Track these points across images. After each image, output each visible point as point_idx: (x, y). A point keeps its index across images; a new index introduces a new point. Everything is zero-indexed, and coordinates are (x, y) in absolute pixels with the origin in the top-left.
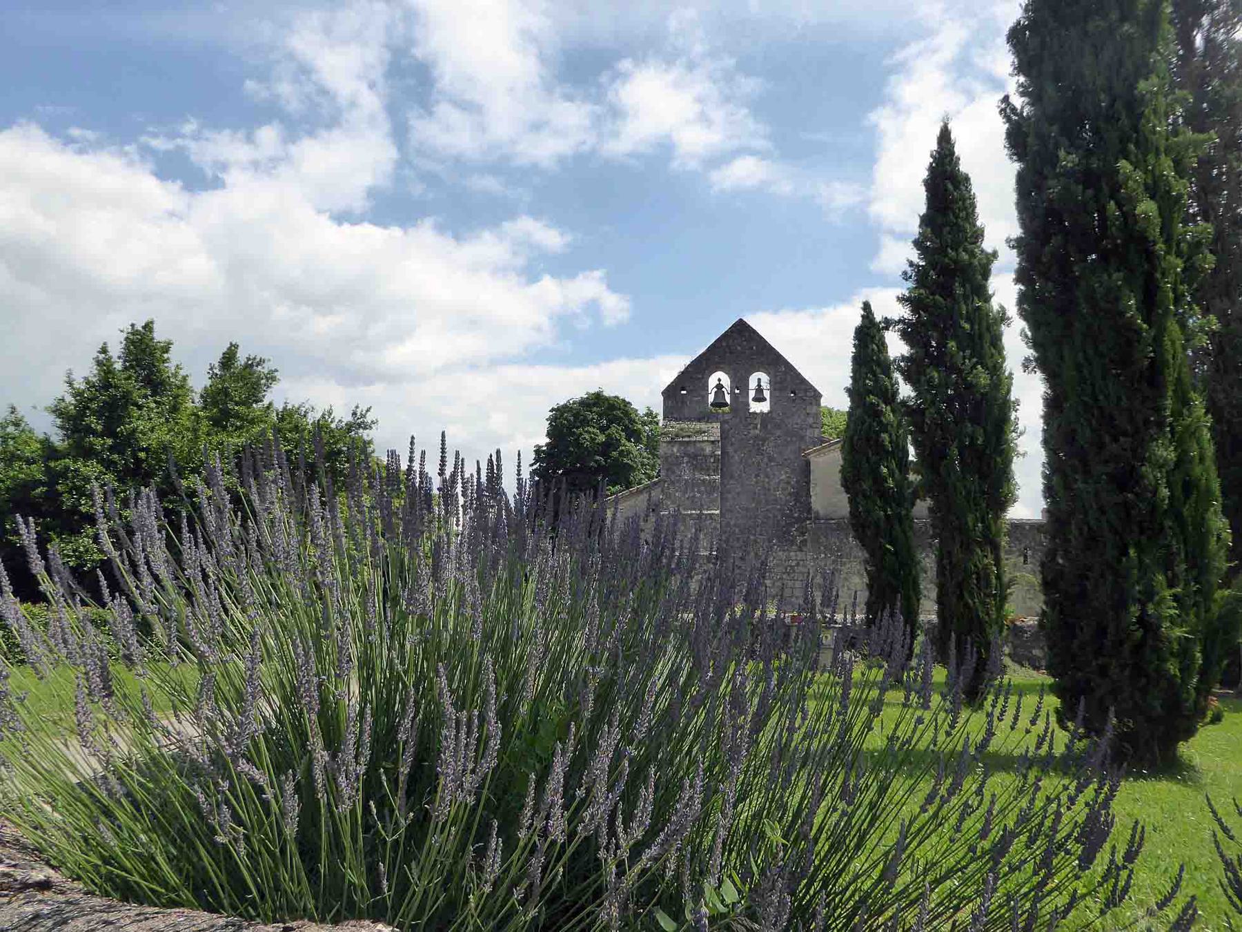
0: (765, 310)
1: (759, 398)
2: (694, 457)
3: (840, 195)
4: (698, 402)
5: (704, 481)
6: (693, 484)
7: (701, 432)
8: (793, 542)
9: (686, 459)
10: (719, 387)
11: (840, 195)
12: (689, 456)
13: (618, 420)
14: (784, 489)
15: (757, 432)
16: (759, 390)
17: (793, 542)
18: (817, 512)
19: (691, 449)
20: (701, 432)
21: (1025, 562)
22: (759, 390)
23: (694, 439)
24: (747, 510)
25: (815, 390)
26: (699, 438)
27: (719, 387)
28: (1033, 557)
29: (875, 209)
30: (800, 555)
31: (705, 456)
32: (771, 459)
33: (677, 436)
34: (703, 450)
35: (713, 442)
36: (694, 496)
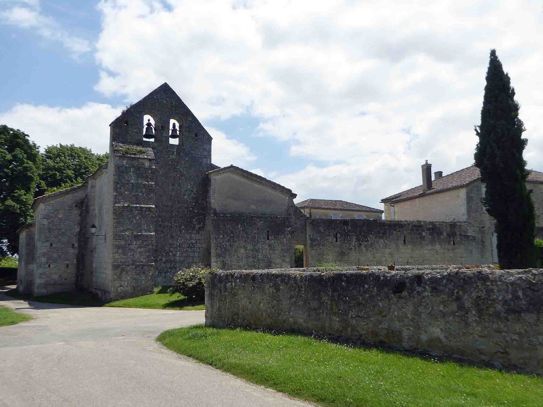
0: (29, 103)
1: (174, 136)
2: (138, 168)
3: (77, 46)
4: (136, 133)
5: (145, 185)
6: (136, 186)
7: (141, 152)
8: (194, 229)
9: (132, 170)
10: (149, 124)
11: (77, 46)
12: (134, 167)
13: (18, 145)
14: (189, 195)
15: (174, 157)
16: (174, 130)
17: (194, 229)
18: (215, 210)
19: (135, 163)
20: (141, 152)
21: (337, 241)
22: (174, 130)
23: (138, 156)
24: (167, 206)
25: (209, 135)
26: (141, 156)
27: (149, 124)
28: (340, 237)
29: (99, 56)
30: (198, 237)
31: (145, 169)
32: (182, 175)
33: (127, 153)
34: (143, 164)
35: (150, 160)
36: (138, 195)
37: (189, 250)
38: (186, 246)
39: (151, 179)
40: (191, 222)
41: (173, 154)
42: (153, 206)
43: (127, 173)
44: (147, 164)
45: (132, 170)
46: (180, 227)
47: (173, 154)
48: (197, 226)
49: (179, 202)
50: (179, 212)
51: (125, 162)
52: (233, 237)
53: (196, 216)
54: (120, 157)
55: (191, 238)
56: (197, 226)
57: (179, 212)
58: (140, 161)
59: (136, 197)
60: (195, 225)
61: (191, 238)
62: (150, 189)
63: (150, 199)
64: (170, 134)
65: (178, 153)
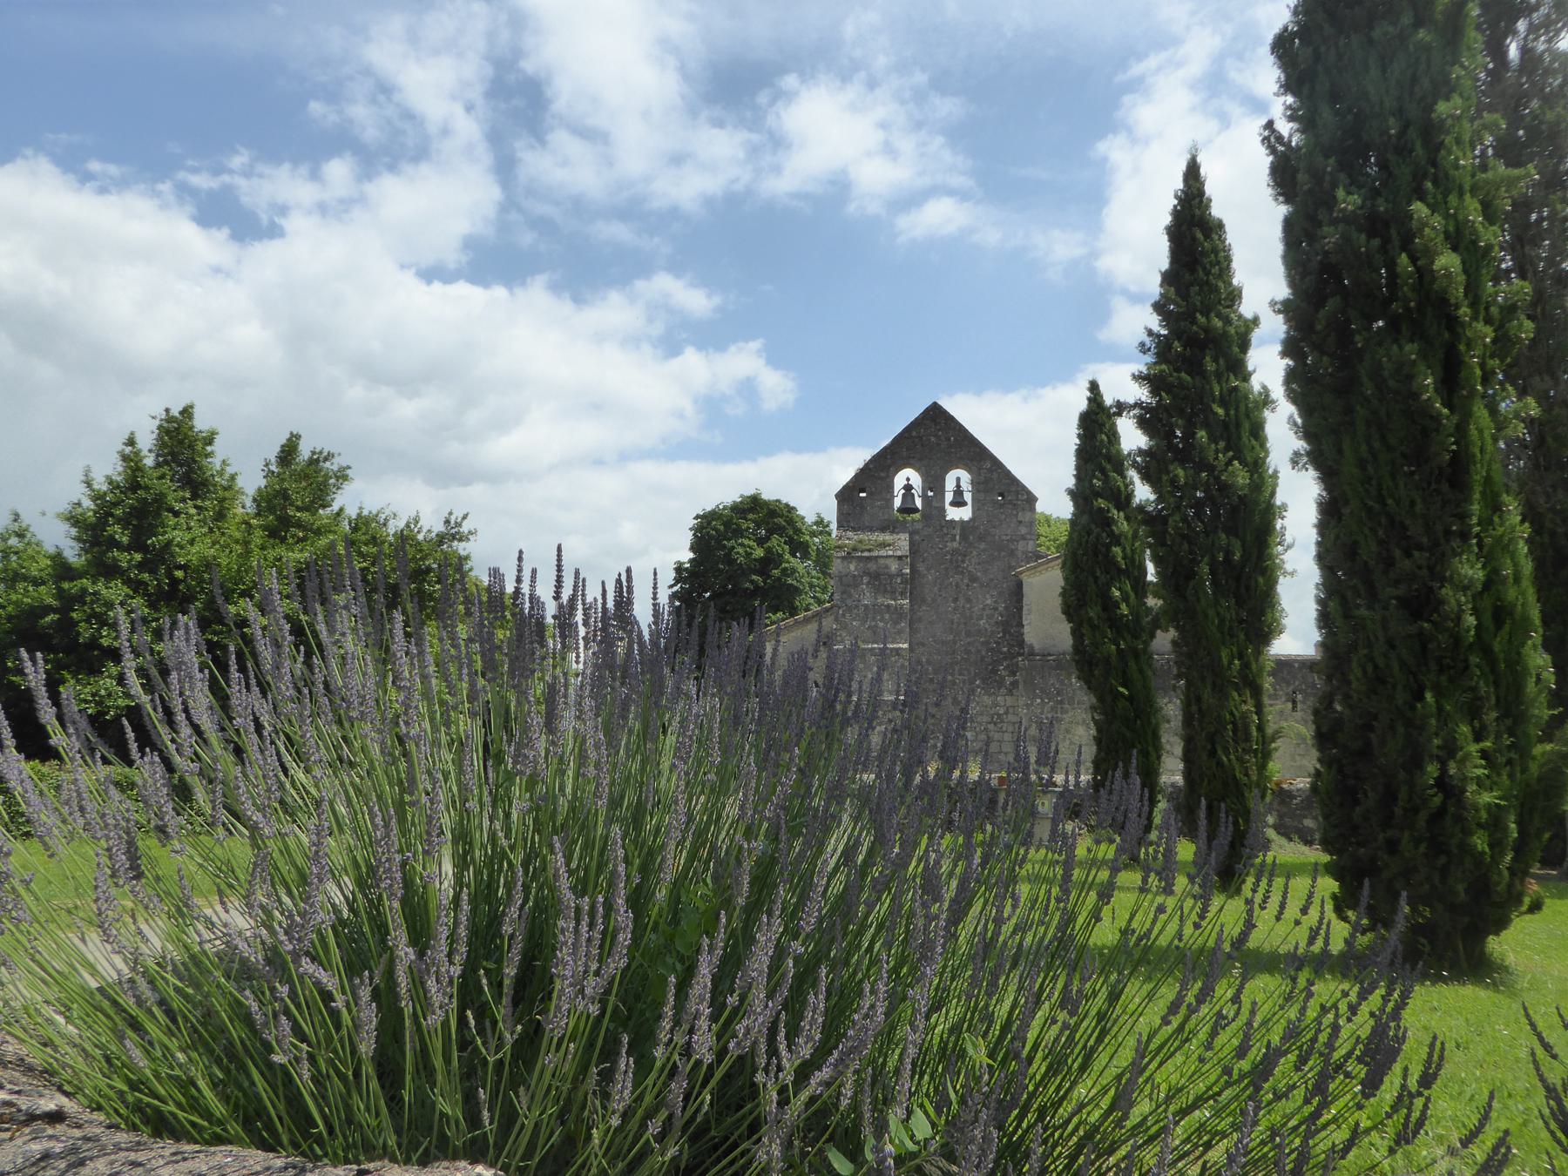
1: (958, 502)
5: (888, 606)
7: (884, 545)
8: (1001, 684)
9: (865, 580)
10: (908, 488)
12: (869, 574)
13: (779, 530)
14: (990, 617)
15: (955, 545)
16: (958, 492)
19: (872, 567)
20: (884, 545)
21: (1294, 709)
22: (958, 492)
23: (876, 553)
25: (1029, 493)
26: (883, 553)
31: (891, 576)
32: (973, 579)
33: (855, 549)
34: (887, 567)
35: (900, 558)
37: (991, 727)
38: (986, 719)
39: (902, 594)
40: (994, 671)
41: (954, 539)
42: (906, 646)
43: (856, 586)
44: (894, 567)
45: (865, 580)
46: (972, 683)
47: (954, 539)
48: (1008, 680)
49: (968, 634)
50: (968, 652)
51: (852, 567)
52: (1061, 702)
53: (1005, 659)
54: (843, 558)
55: (996, 705)
56: (1008, 680)
57: (968, 652)
58: (882, 561)
59: (874, 630)
60: (1003, 678)
61: (996, 705)
62: (898, 613)
63: (900, 632)
64: (126, 722)
65: (964, 537)
